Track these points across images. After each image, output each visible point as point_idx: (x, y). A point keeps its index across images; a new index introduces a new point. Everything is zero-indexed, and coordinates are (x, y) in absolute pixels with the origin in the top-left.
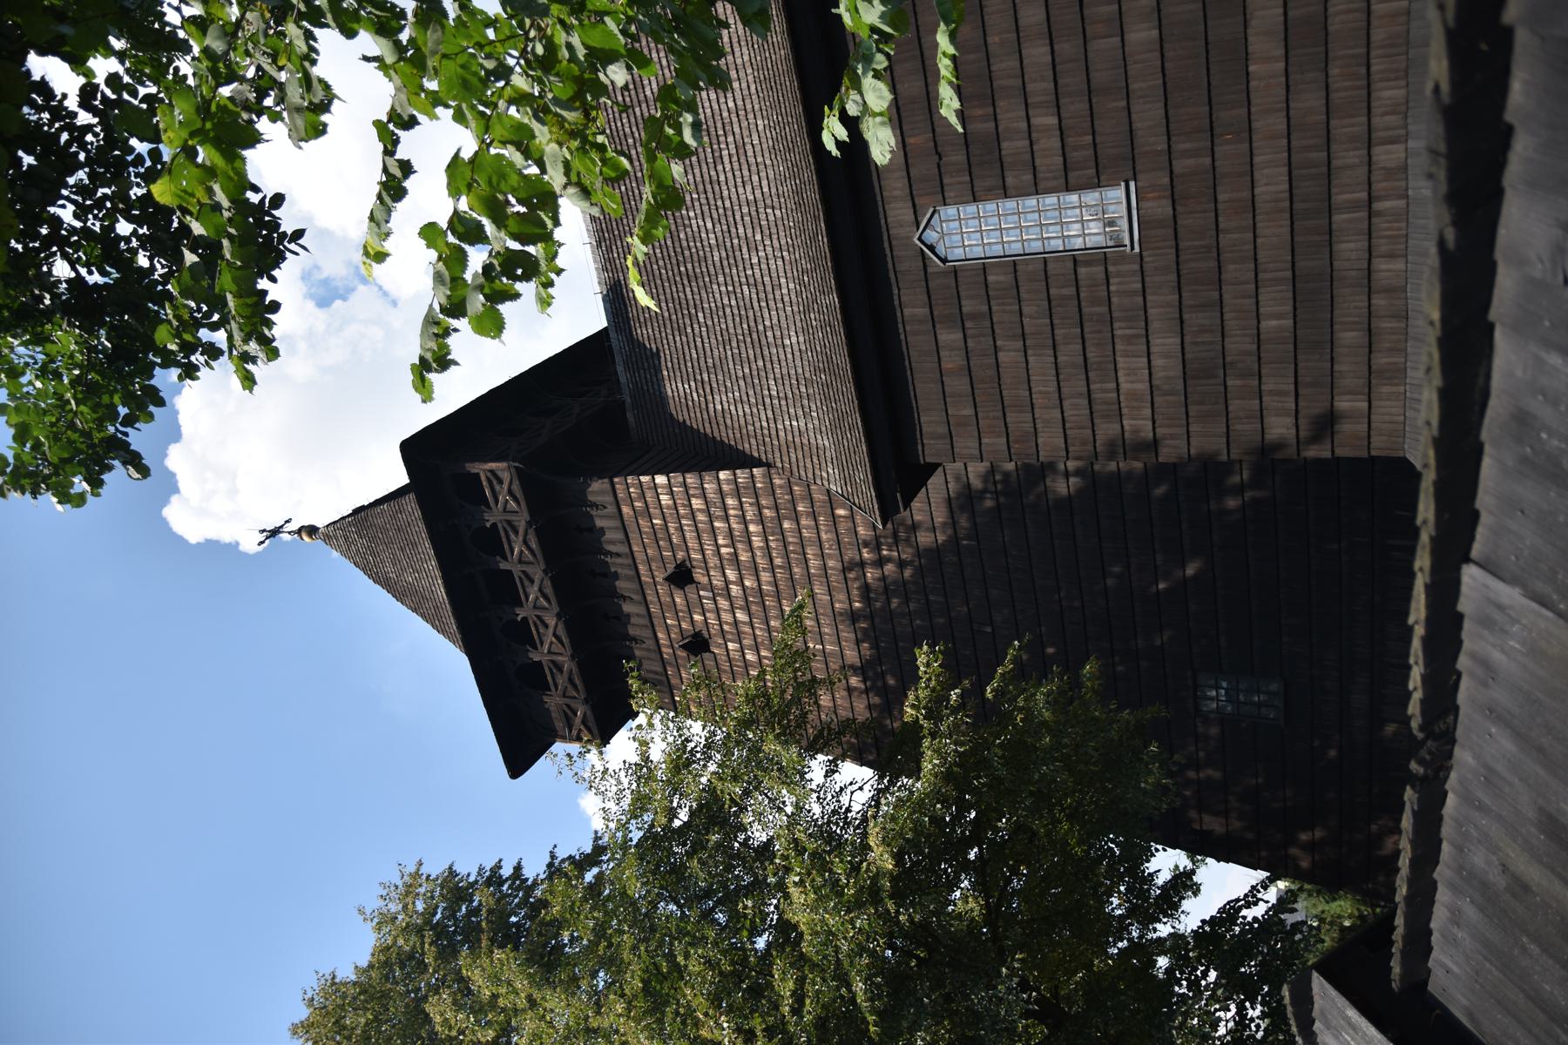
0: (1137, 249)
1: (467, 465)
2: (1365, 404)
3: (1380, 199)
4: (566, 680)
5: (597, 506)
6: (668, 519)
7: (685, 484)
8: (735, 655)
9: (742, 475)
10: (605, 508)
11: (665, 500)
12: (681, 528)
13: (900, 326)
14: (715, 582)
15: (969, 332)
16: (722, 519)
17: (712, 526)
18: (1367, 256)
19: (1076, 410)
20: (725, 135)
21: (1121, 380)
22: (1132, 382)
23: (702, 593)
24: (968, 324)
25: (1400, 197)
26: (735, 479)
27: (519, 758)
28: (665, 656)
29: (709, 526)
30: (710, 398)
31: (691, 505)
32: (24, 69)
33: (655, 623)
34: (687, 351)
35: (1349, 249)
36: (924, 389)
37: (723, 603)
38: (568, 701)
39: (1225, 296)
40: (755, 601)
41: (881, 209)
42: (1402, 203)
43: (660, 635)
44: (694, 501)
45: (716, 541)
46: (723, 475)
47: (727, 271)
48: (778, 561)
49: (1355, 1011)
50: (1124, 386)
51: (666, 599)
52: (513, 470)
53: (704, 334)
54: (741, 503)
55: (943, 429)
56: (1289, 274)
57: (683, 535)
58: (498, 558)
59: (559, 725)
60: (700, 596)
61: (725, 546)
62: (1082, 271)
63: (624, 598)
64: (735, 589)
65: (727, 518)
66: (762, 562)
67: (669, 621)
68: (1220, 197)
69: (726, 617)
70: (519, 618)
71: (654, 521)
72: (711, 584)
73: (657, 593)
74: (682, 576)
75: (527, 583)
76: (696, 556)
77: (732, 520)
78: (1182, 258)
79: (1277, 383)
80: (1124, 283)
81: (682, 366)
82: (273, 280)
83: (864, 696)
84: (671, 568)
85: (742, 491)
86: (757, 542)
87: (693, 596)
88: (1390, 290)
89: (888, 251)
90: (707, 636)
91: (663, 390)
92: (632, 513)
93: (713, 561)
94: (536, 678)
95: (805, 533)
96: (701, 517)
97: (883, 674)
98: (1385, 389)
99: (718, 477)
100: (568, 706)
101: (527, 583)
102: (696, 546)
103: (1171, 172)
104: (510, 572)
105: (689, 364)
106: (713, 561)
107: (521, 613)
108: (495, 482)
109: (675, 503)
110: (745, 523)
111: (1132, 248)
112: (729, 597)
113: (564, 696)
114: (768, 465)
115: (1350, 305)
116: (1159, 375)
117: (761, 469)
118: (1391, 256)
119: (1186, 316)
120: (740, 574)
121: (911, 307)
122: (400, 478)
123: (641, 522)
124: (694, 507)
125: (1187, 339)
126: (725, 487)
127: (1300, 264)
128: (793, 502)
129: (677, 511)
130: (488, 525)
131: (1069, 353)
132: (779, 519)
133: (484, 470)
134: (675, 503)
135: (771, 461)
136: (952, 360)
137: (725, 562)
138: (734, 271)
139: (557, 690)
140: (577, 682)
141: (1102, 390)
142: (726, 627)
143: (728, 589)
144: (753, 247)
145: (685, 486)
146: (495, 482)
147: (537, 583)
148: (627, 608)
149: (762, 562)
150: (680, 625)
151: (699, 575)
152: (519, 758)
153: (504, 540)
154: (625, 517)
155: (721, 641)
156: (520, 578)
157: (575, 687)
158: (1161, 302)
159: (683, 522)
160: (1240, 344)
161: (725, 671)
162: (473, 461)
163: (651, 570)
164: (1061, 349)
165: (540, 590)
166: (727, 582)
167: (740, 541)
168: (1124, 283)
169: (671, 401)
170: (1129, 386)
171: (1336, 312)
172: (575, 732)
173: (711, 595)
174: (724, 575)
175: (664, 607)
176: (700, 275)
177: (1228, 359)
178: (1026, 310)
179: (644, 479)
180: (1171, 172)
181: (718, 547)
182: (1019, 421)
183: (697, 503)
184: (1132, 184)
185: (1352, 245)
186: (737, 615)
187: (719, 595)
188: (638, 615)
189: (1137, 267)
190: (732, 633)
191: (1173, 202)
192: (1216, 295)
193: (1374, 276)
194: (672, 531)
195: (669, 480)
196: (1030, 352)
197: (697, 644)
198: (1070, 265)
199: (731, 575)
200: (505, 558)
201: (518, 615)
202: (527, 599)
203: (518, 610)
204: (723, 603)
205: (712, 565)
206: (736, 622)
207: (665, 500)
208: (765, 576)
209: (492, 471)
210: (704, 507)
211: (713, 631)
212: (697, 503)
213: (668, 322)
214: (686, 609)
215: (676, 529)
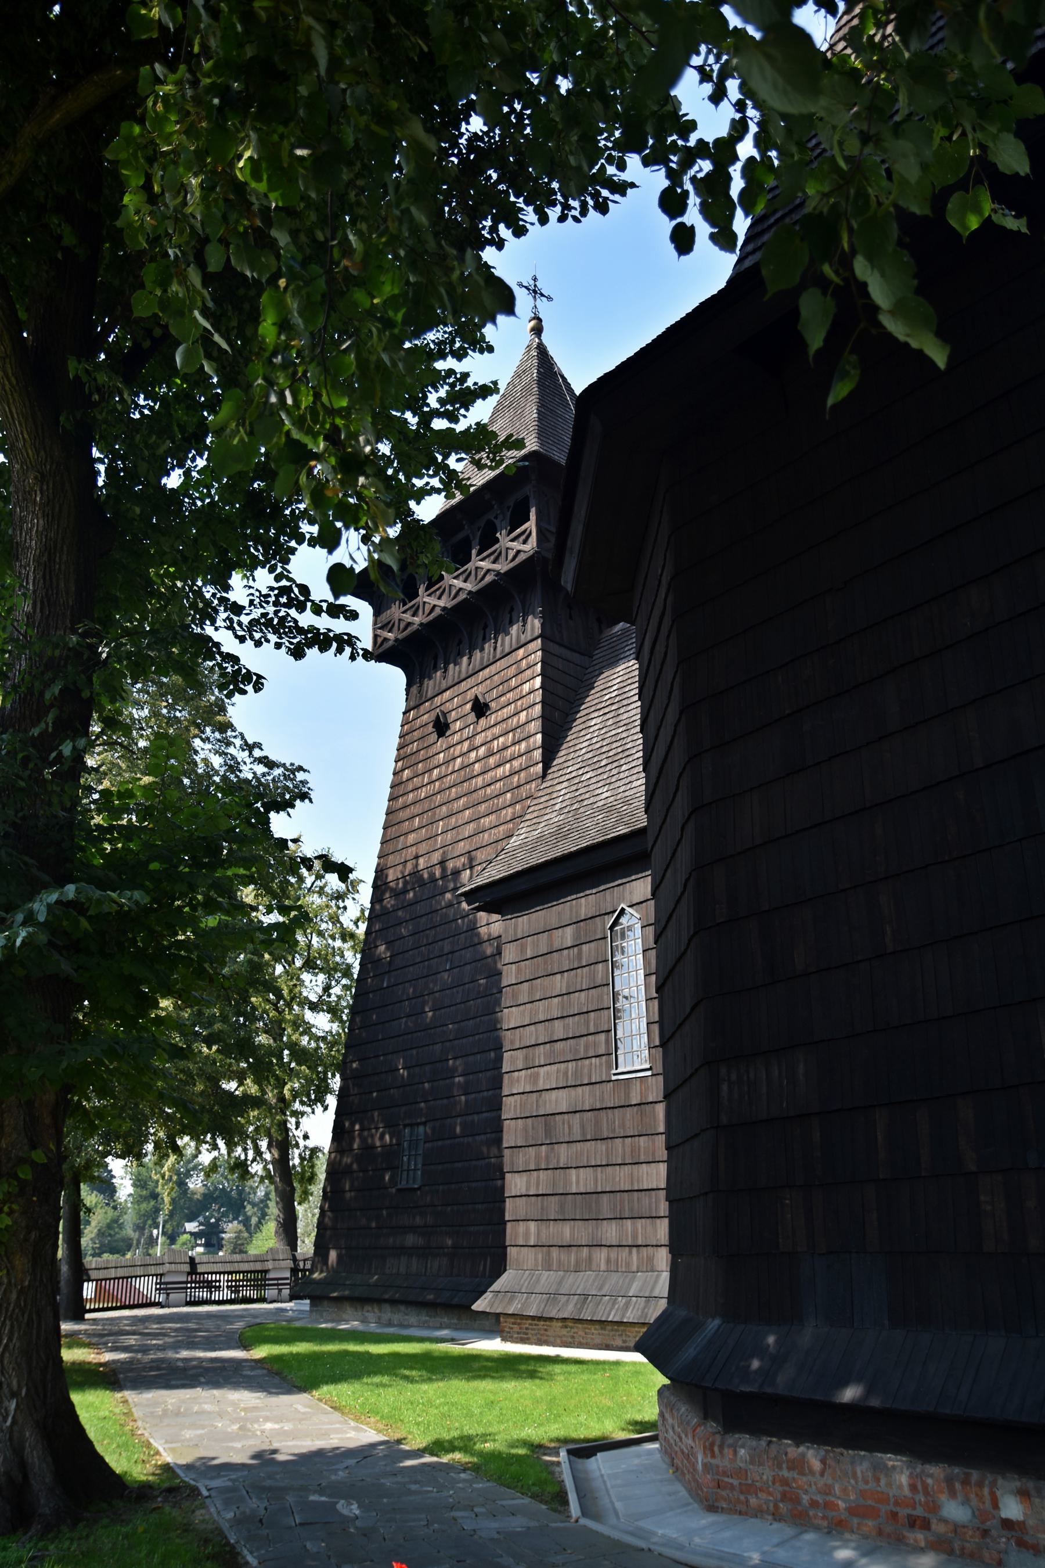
0: (614, 1078)
2: (532, 1244)
3: (638, 1253)
5: (445, 672)
8: (435, 761)
9: (538, 754)
13: (574, 897)
15: (571, 950)
21: (545, 1068)
24: (576, 949)
25: (638, 1267)
32: (443, 373)
35: (611, 1232)
38: (473, 573)
39: (588, 1143)
41: (640, 875)
42: (634, 1269)
44: (525, 713)
50: (542, 1070)
56: (599, 1190)
62: (603, 1036)
63: (470, 658)
64: (473, 755)
68: (642, 1139)
75: (492, 558)
78: (609, 1111)
79: (543, 1181)
80: (594, 1069)
82: (418, 503)
88: (590, 1259)
89: (617, 883)
90: (447, 734)
91: (621, 662)
97: (413, 889)
98: (540, 1256)
101: (492, 558)
103: (656, 1102)
108: (524, 537)
111: (615, 1074)
113: (400, 620)
114: (544, 775)
115: (581, 1232)
117: (541, 770)
118: (608, 1261)
119: (578, 1115)
121: (585, 903)
125: (566, 1116)
127: (605, 1197)
135: (549, 777)
137: (488, 745)
140: (409, 629)
141: (540, 1054)
146: (524, 537)
148: (514, 629)
151: (483, 722)
157: (405, 629)
158: (585, 1097)
160: (564, 1154)
165: (488, 571)
168: (594, 1069)
169: (612, 672)
170: (542, 1075)
171: (580, 1222)
177: (556, 1146)
178: (583, 994)
180: (656, 1102)
184: (649, 1073)
185: (614, 1234)
188: (460, 672)
189: (604, 1079)
191: (639, 1104)
192: (589, 1137)
193: (598, 1248)
196: (560, 998)
198: (606, 1029)
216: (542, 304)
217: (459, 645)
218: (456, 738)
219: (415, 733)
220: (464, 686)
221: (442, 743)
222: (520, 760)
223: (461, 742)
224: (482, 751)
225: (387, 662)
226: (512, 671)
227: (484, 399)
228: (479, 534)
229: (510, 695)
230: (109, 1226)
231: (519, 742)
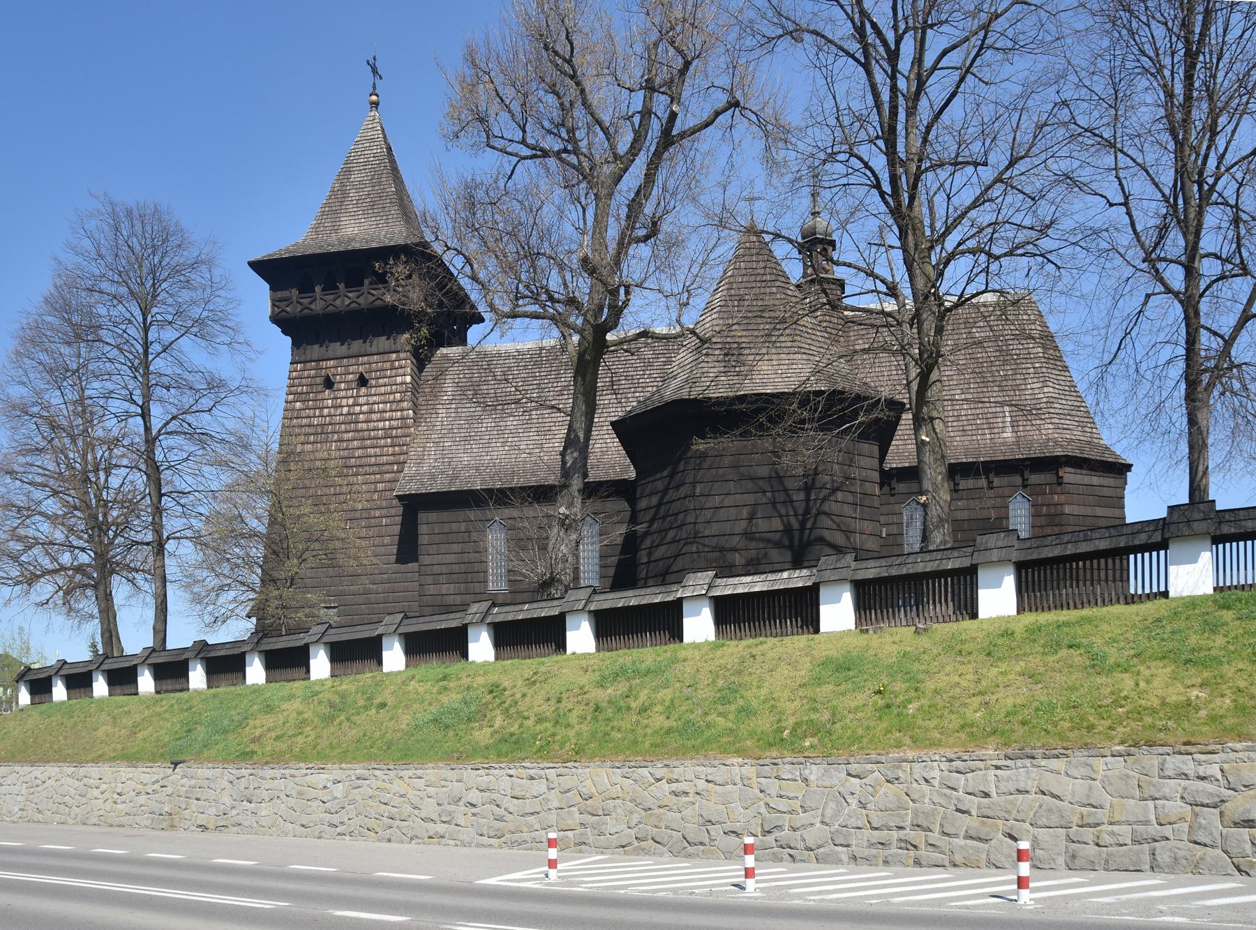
11: (399, 379)
18: (381, 351)
19: (436, 569)
20: (402, 410)
22: (445, 589)
27: (262, 267)
36: (445, 515)
37: (351, 401)
40: (352, 419)
48: (372, 433)
49: (169, 681)
51: (351, 369)
55: (430, 521)
64: (357, 409)
65: (391, 411)
66: (372, 425)
69: (344, 402)
74: (363, 381)
83: (88, 603)
84: (367, 376)
86: (381, 425)
93: (372, 399)
94: (306, 289)
95: (385, 449)
96: (392, 397)
106: (372, 399)
107: (341, 286)
110: (390, 420)
112: (354, 405)
116: (447, 597)
128: (399, 445)
131: (456, 568)
132: (391, 437)
136: (455, 526)
141: (443, 579)
145: (400, 401)
149: (372, 425)
151: (363, 390)
152: (262, 267)
164: (457, 566)
179: (409, 370)
181: (378, 403)
182: (433, 549)
197: (329, 384)
199: (365, 408)
204: (351, 401)
206: (342, 407)
208: (364, 426)
216: (378, 82)
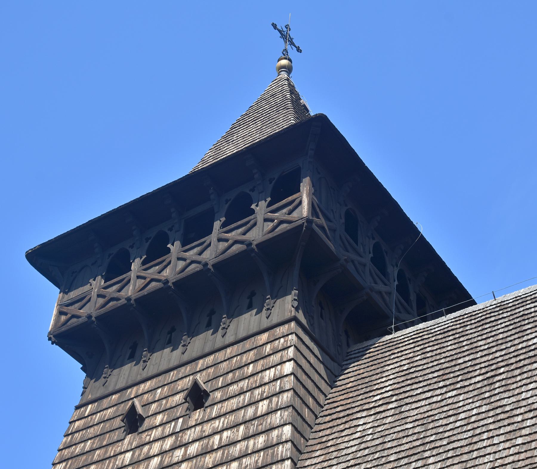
1: (308, 178)
4: (112, 296)
6: (252, 379)
7: (282, 392)
9: (285, 450)
10: (267, 318)
11: (269, 374)
12: (242, 393)
14: (189, 432)
16: (245, 434)
17: (241, 424)
23: (181, 420)
26: (282, 443)
28: (129, 390)
29: (241, 421)
30: (373, 412)
31: (262, 400)
33: (160, 378)
34: (421, 385)
43: (148, 383)
44: (266, 402)
45: (227, 429)
46: (287, 430)
47: (491, 413)
52: (300, 222)
53: (435, 399)
54: (258, 451)
57: (236, 396)
58: (269, 199)
59: (74, 294)
60: (178, 418)
61: (221, 439)
64: (179, 454)
65: (246, 438)
67: (159, 391)
70: (169, 246)
71: (251, 365)
72: (188, 429)
73: (186, 377)
76: (215, 411)
77: (244, 444)
81: (409, 382)
85: (270, 451)
87: (180, 411)
90: (140, 430)
92: (261, 343)
99: (285, 424)
100: (89, 300)
102: (224, 410)
104: (210, 232)
105: (408, 388)
108: (290, 207)
109: (265, 384)
112: (173, 449)
120: (193, 457)
122: (312, 113)
123: (252, 353)
124: (261, 404)
126: (275, 433)
129: (258, 387)
130: (253, 206)
133: (301, 197)
134: (265, 384)
137: (205, 441)
138: (491, 420)
139: (340, 236)
142: (146, 449)
143: (180, 447)
144: (509, 438)
145: (280, 393)
147: (199, 258)
150: (155, 402)
151: (198, 415)
153: (239, 223)
154: (259, 337)
155: (134, 444)
156: (248, 222)
159: (248, 394)
161: (106, 452)
162: (313, 185)
163: (208, 368)
166: (186, 445)
167: (223, 454)
172: (65, 309)
173: (178, 430)
174: (194, 441)
175: (172, 385)
176: (492, 387)
183: (263, 406)
186: (156, 458)
187: (177, 438)
190: (140, 455)
194: (241, 384)
195: (287, 375)
200: (224, 225)
201: (173, 245)
202: (227, 232)
203: (177, 243)
204: (168, 443)
205: (205, 428)
207: (269, 374)
209: (300, 203)
210: (259, 413)
211: (144, 435)
212: (263, 406)
213: (453, 363)
214: (168, 406)
215: (242, 388)
217: (170, 333)
218: (156, 433)
219: (91, 430)
220: (172, 375)
221: (129, 440)
222: (254, 457)
223: (163, 438)
224: (193, 449)
225: (58, 346)
226: (251, 355)
227: (81, 368)
228: (227, 206)
229: (244, 384)
230: (207, 386)
231: (254, 436)
